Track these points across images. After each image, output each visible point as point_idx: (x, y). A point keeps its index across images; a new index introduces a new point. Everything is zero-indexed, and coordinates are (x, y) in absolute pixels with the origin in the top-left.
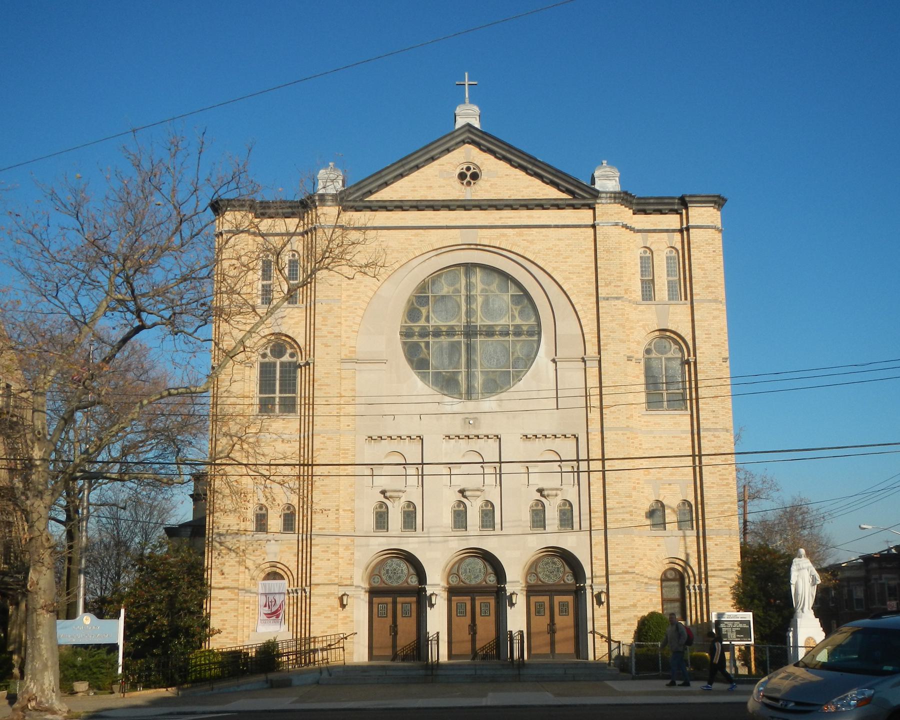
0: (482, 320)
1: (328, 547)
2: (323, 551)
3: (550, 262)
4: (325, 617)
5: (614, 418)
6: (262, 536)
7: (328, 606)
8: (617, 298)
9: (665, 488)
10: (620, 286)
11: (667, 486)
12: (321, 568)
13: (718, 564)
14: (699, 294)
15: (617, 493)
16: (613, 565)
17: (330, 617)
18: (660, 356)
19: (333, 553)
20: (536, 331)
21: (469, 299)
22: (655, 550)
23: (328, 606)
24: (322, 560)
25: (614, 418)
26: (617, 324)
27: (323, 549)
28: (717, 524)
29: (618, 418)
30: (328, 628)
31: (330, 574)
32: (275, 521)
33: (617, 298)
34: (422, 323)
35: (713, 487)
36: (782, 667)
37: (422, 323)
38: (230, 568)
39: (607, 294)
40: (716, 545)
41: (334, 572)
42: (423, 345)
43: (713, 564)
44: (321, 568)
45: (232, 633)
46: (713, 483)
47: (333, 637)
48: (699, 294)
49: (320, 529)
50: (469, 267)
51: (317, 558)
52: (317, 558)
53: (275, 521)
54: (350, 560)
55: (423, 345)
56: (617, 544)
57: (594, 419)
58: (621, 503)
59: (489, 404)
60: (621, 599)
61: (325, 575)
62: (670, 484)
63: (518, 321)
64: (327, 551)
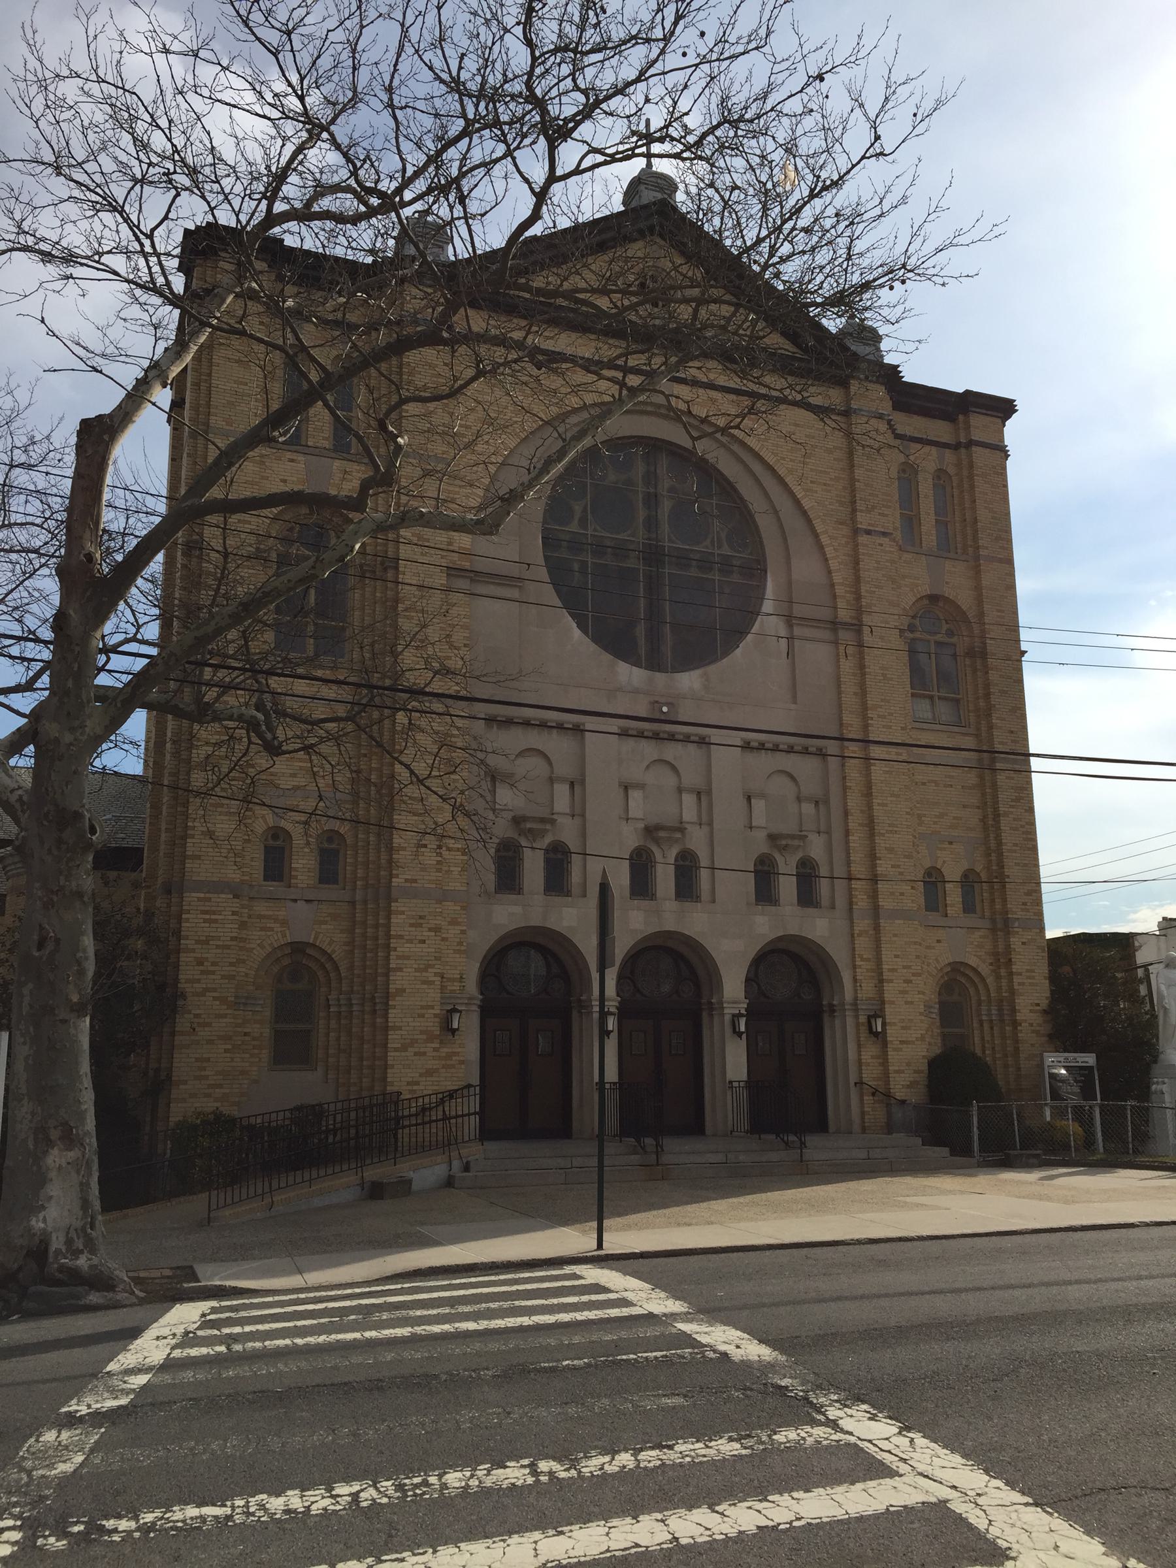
0: (670, 540)
1: (421, 917)
2: (411, 925)
3: (784, 459)
4: (416, 1054)
5: (884, 727)
6: (272, 887)
7: (422, 1032)
8: (884, 534)
9: (944, 849)
10: (887, 515)
11: (946, 845)
12: (408, 958)
13: (207, 1073)
14: (987, 548)
15: (890, 850)
16: (889, 970)
17: (424, 1054)
18: (929, 637)
19: (430, 930)
20: (756, 570)
21: (652, 501)
22: (934, 948)
23: (422, 1032)
24: (410, 941)
25: (884, 727)
26: (883, 576)
27: (412, 921)
28: (1022, 910)
29: (890, 727)
30: (421, 1075)
31: (425, 970)
32: (954, 896)
33: (884, 534)
34: (574, 527)
35: (1015, 851)
36: (668, 1207)
37: (574, 527)
38: (219, 951)
39: (869, 525)
40: (1023, 943)
41: (432, 966)
42: (576, 567)
43: (1020, 974)
44: (408, 958)
45: (220, 1086)
46: (1015, 845)
47: (288, 1114)
48: (987, 548)
49: (406, 880)
50: (654, 446)
51: (401, 937)
52: (401, 937)
53: (954, 896)
54: (460, 943)
55: (576, 567)
56: (895, 935)
57: (851, 725)
58: (899, 866)
59: (689, 681)
60: (903, 1028)
61: (417, 970)
62: (951, 843)
63: (726, 550)
64: (421, 925)
